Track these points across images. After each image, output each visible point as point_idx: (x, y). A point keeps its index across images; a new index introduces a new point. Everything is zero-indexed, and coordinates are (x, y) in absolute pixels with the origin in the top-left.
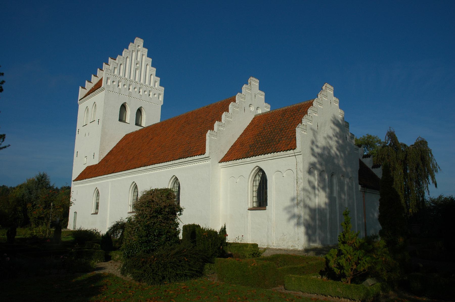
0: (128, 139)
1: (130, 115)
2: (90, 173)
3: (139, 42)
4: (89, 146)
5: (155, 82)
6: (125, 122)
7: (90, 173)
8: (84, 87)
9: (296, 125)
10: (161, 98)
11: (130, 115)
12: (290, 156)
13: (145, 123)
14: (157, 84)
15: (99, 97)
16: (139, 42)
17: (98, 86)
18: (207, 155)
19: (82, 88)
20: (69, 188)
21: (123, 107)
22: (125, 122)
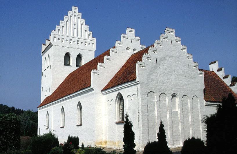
0: (72, 76)
1: (73, 61)
2: (50, 100)
3: (75, 9)
4: (53, 74)
5: (89, 35)
6: (69, 65)
7: (50, 100)
8: (44, 45)
9: (158, 138)
10: (94, 46)
11: (73, 61)
12: (209, 106)
13: (83, 62)
14: (91, 37)
15: (50, 51)
16: (75, 9)
17: (50, 45)
18: (137, 80)
19: (43, 45)
20: (37, 113)
21: (67, 56)
22: (69, 65)
